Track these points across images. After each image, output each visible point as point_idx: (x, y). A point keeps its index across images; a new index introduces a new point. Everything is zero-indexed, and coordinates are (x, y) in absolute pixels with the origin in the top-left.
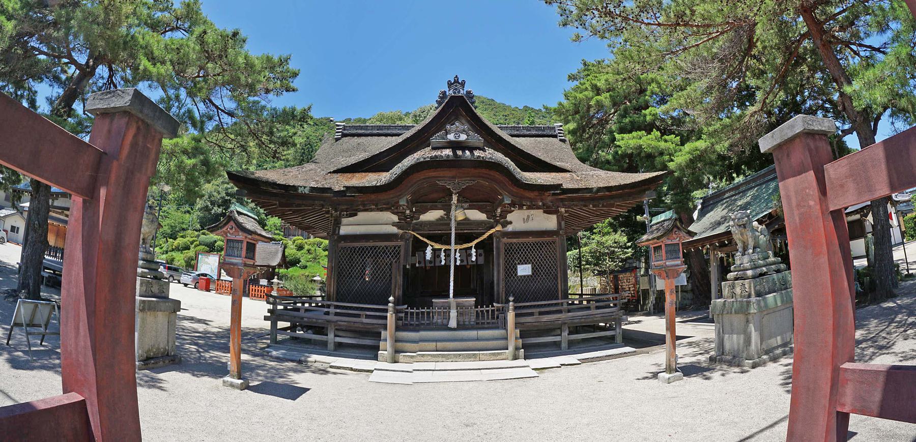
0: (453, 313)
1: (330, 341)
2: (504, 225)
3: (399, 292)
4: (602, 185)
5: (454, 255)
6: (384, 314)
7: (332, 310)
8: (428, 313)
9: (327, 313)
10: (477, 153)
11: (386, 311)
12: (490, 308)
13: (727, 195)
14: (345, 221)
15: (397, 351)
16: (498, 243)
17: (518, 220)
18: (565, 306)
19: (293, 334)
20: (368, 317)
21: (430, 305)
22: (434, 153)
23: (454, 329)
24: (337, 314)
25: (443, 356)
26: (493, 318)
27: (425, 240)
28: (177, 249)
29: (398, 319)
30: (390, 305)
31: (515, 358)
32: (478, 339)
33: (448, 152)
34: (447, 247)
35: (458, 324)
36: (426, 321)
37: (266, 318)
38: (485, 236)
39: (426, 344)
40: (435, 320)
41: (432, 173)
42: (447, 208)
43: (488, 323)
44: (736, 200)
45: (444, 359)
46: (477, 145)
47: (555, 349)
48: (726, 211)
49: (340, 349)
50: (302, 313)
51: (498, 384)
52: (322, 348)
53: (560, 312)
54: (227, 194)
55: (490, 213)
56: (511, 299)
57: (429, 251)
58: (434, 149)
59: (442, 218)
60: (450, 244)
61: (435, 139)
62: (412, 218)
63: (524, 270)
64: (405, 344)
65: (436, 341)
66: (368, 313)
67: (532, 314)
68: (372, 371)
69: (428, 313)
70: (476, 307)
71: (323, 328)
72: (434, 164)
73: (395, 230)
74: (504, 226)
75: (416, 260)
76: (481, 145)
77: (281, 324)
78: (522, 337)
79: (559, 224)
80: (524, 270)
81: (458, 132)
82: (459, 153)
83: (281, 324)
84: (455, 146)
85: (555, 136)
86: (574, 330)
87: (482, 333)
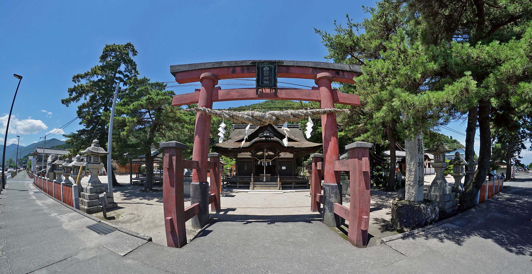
0: (265, 178)
3: (254, 172)
5: (265, 163)
15: (254, 187)
17: (283, 155)
21: (259, 176)
33: (264, 138)
42: (264, 152)
47: (290, 188)
49: (240, 188)
52: (236, 188)
55: (275, 153)
61: (260, 135)
63: (284, 168)
77: (225, 183)
78: (282, 184)
80: (284, 168)
81: (267, 133)
83: (225, 183)
84: (266, 137)
86: (297, 184)
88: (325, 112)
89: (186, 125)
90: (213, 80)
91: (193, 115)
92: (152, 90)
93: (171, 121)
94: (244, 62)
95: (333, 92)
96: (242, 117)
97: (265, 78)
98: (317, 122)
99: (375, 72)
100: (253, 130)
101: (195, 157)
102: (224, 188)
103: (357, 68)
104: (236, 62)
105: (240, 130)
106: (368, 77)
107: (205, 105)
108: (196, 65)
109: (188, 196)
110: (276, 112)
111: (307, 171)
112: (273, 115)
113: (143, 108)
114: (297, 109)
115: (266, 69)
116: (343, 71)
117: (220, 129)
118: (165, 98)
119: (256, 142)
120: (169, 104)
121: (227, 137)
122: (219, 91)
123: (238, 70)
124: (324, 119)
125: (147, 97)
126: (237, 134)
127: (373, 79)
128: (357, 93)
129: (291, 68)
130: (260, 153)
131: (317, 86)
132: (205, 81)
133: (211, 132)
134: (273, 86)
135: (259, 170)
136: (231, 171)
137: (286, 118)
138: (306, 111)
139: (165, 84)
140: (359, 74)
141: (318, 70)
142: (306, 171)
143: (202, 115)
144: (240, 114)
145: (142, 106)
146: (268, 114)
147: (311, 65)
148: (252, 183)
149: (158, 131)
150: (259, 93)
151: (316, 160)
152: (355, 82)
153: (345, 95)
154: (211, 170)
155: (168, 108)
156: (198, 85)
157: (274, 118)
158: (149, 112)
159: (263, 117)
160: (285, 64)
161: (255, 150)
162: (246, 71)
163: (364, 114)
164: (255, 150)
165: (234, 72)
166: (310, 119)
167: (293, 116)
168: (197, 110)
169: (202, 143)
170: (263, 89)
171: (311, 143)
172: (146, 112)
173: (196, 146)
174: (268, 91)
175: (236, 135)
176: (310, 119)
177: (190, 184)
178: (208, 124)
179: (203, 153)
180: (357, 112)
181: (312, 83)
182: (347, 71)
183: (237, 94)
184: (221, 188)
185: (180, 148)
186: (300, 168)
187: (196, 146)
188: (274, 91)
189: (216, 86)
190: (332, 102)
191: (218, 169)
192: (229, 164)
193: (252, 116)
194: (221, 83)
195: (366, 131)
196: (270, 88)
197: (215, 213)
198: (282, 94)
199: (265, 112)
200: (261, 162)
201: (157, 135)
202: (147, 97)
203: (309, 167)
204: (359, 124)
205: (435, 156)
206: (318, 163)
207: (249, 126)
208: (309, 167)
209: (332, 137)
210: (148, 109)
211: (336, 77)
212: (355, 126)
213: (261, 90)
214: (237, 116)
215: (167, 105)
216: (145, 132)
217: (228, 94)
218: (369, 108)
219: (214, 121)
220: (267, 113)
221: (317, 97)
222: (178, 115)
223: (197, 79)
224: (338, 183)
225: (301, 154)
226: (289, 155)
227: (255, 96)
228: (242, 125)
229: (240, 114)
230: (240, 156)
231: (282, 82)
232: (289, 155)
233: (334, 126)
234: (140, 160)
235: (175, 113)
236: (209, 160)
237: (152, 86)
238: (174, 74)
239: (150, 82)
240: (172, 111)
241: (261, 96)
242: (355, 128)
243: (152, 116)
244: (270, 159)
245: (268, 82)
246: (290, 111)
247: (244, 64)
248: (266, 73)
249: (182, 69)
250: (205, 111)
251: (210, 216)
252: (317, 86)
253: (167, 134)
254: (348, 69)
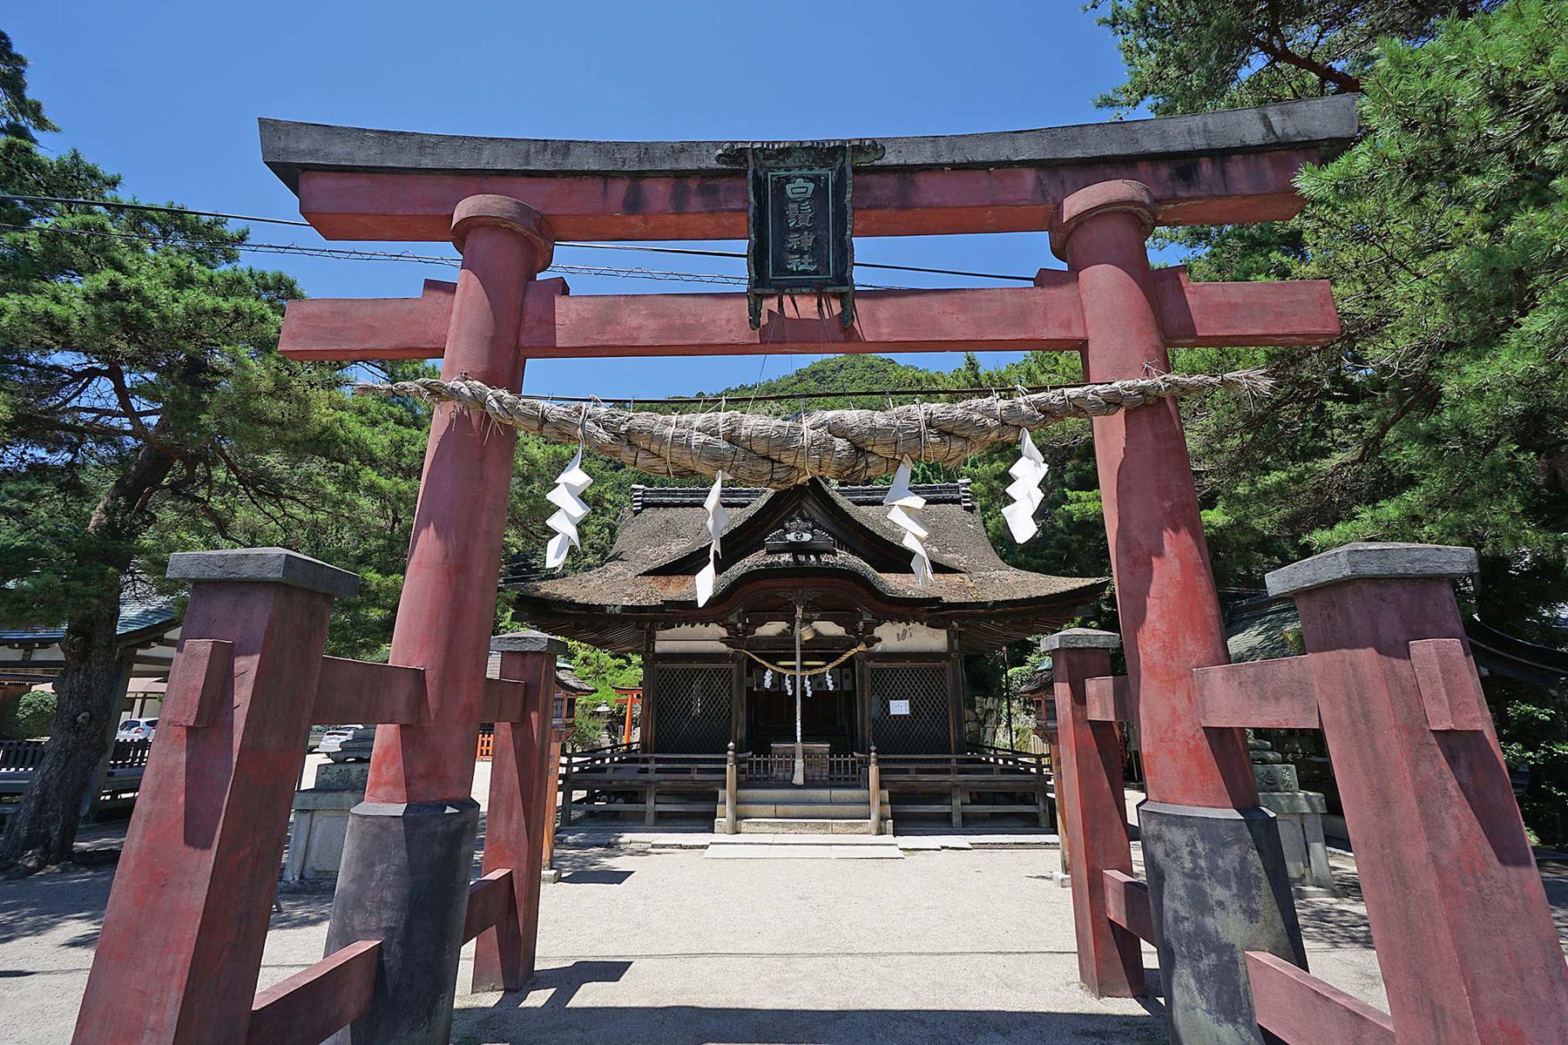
0: (799, 764)
3: (741, 733)
4: (1001, 598)
5: (799, 680)
7: (652, 766)
8: (766, 763)
9: (646, 771)
10: (824, 558)
11: (725, 761)
12: (849, 759)
13: (1274, 608)
14: (660, 634)
17: (890, 636)
18: (954, 764)
19: (590, 807)
20: (700, 771)
21: (767, 751)
22: (770, 559)
24: (658, 771)
29: (740, 772)
31: (881, 832)
32: (831, 803)
33: (786, 557)
36: (762, 775)
41: (769, 583)
42: (791, 621)
44: (1285, 620)
46: (825, 547)
47: (942, 824)
48: (1262, 637)
49: (666, 822)
50: (609, 775)
51: (850, 862)
52: (636, 822)
53: (947, 771)
57: (768, 676)
58: (769, 553)
62: (745, 632)
63: (900, 707)
67: (906, 771)
69: (766, 763)
71: (636, 793)
72: (770, 572)
73: (723, 647)
75: (751, 682)
76: (830, 547)
77: (578, 795)
78: (895, 799)
79: (950, 642)
80: (900, 707)
81: (799, 531)
82: (802, 558)
83: (578, 795)
84: (796, 548)
85: (958, 501)
86: (979, 798)
87: (837, 793)
88: (1112, 403)
89: (369, 475)
90: (527, 243)
91: (418, 423)
92: (136, 248)
93: (277, 442)
94: (684, 148)
95: (1160, 289)
96: (682, 443)
97: (794, 241)
98: (1071, 467)
99: (1467, 92)
100: (738, 517)
101: (403, 649)
102: (568, 824)
103: (1320, 116)
104: (645, 149)
105: (670, 513)
106: (1412, 145)
107: (481, 368)
108: (423, 142)
109: (316, 886)
110: (852, 416)
111: (1031, 722)
112: (836, 430)
113: (67, 346)
114: (955, 396)
115: (799, 188)
116: (1222, 155)
117: (579, 511)
118: (238, 313)
119: (750, 577)
120: (265, 346)
121: (596, 548)
122: (560, 302)
123: (657, 193)
124: (1111, 440)
125: (103, 278)
126: (656, 537)
127: (1448, 149)
128: (1312, 269)
129: (922, 179)
130: (772, 629)
131: (1064, 266)
132: (481, 242)
133: (515, 522)
134: (834, 279)
135: (768, 720)
136: (616, 721)
137: (905, 442)
138: (1005, 403)
139: (231, 228)
140: (1327, 150)
141: (1066, 174)
142: (1025, 721)
143: (461, 420)
144: (669, 425)
145: (58, 332)
146: (808, 427)
147: (1028, 150)
148: (726, 794)
149: (176, 490)
150: (764, 320)
151: (1078, 665)
152: (1300, 203)
153: (1234, 291)
154: (503, 729)
155: (259, 371)
156: (443, 259)
157: (841, 444)
158: (115, 375)
159: (785, 441)
160: (891, 159)
161: (746, 613)
162: (696, 203)
163: (1353, 394)
164: (746, 613)
165: (634, 204)
166: (1028, 443)
167: (942, 433)
168: (437, 392)
169: (456, 569)
170: (787, 300)
171: (1033, 577)
172: (92, 373)
173: (417, 589)
174: (806, 307)
175: (651, 538)
176: (1028, 443)
177: (344, 811)
178: (491, 463)
179: (460, 631)
180: (1315, 384)
181: (1033, 250)
182: (1246, 150)
183: (652, 324)
184: (551, 823)
185: (312, 593)
186: (990, 703)
187: (417, 589)
188: (836, 306)
189: (540, 277)
190: (1155, 339)
191: (545, 719)
192: (606, 684)
193: (732, 438)
194: (567, 258)
195: (1389, 485)
196: (820, 292)
197: (491, 999)
198: (873, 321)
199: (797, 417)
200: (778, 679)
201: (168, 515)
202: (103, 278)
203: (1039, 697)
204: (1324, 453)
205: (332, 718)
206: (1092, 686)
207: (716, 488)
208: (1039, 697)
209: (1167, 535)
210: (107, 354)
211: (1174, 199)
212: (1296, 469)
213: (771, 304)
214: (652, 437)
215: (244, 351)
216: (82, 492)
217: (604, 323)
218: (1403, 344)
219: (533, 463)
220: (806, 423)
221: (1068, 325)
222: (322, 414)
223: (435, 226)
224: (1248, 807)
225: (985, 642)
226: (928, 639)
227: (743, 334)
228: (678, 485)
229: (669, 425)
230: (670, 641)
231: (877, 258)
232: (928, 639)
233: (1170, 482)
234: (16, 655)
235: (304, 402)
236: (493, 669)
237: (136, 226)
238: (290, 174)
239: (124, 195)
240: (281, 389)
241: (775, 337)
242: (1299, 479)
243: (137, 404)
244: (828, 658)
245: (806, 264)
246: (920, 411)
247: (686, 164)
248: (799, 215)
249: (339, 153)
250: (479, 400)
251: (459, 1029)
252: (1064, 266)
253: (242, 514)
254: (1253, 133)
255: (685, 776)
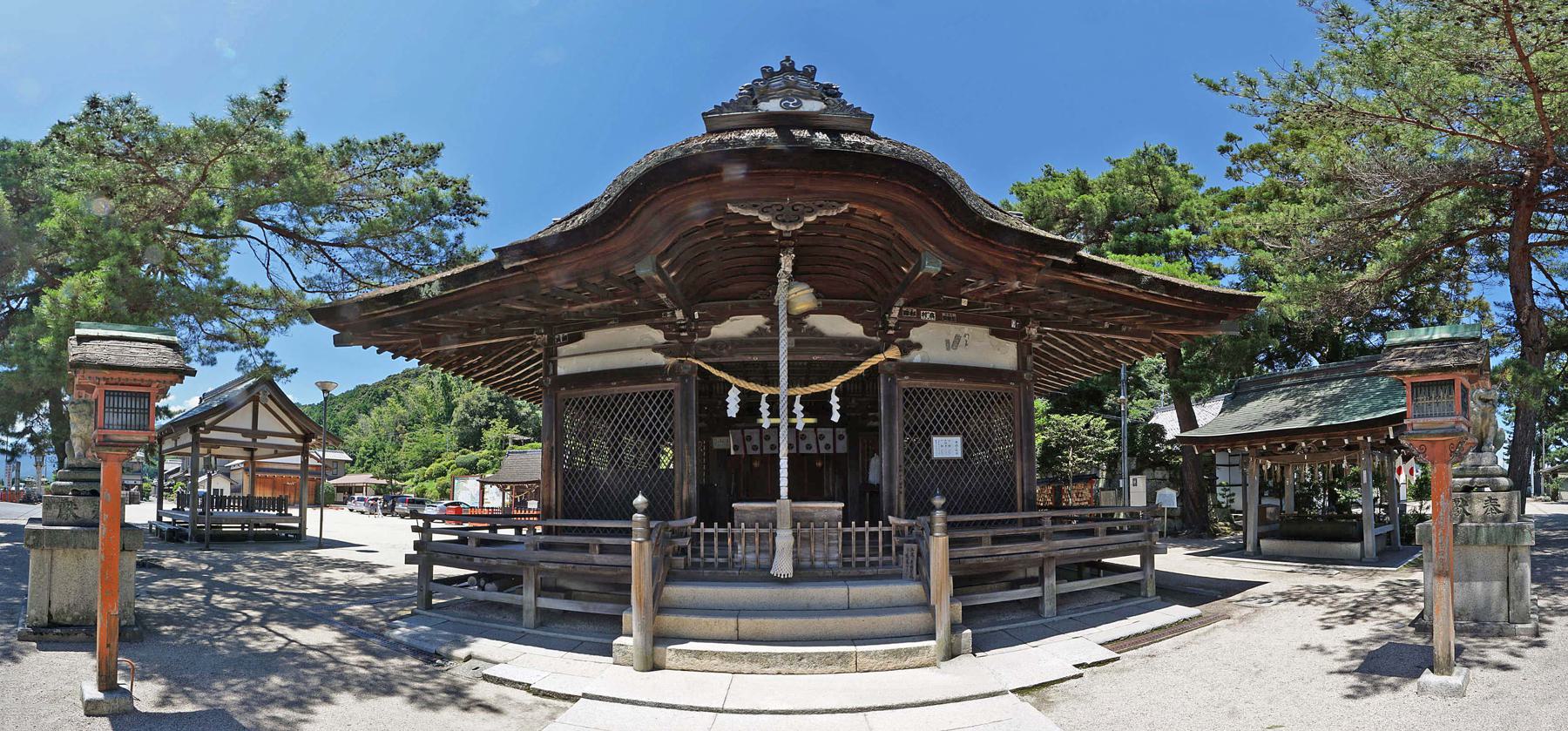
0: (784, 538)
1: (526, 607)
2: (907, 348)
6: (625, 541)
11: (627, 533)
12: (880, 528)
14: (563, 350)
16: (891, 386)
17: (935, 341)
18: (1048, 525)
20: (604, 549)
21: (727, 517)
23: (785, 582)
25: (754, 658)
26: (887, 551)
27: (724, 375)
28: (430, 477)
30: (637, 517)
31: (951, 653)
34: (773, 390)
35: (796, 568)
37: (409, 560)
38: (861, 369)
39: (711, 620)
40: (739, 556)
43: (873, 564)
45: (756, 667)
53: (1035, 538)
54: (491, 400)
55: (875, 322)
56: (938, 501)
59: (760, 331)
60: (776, 384)
63: (947, 447)
64: (683, 618)
65: (738, 611)
66: (605, 540)
68: (573, 699)
69: (723, 537)
70: (846, 524)
74: (904, 352)
80: (947, 447)
83: (440, 571)
200: (750, 404)
255: (579, 557)
